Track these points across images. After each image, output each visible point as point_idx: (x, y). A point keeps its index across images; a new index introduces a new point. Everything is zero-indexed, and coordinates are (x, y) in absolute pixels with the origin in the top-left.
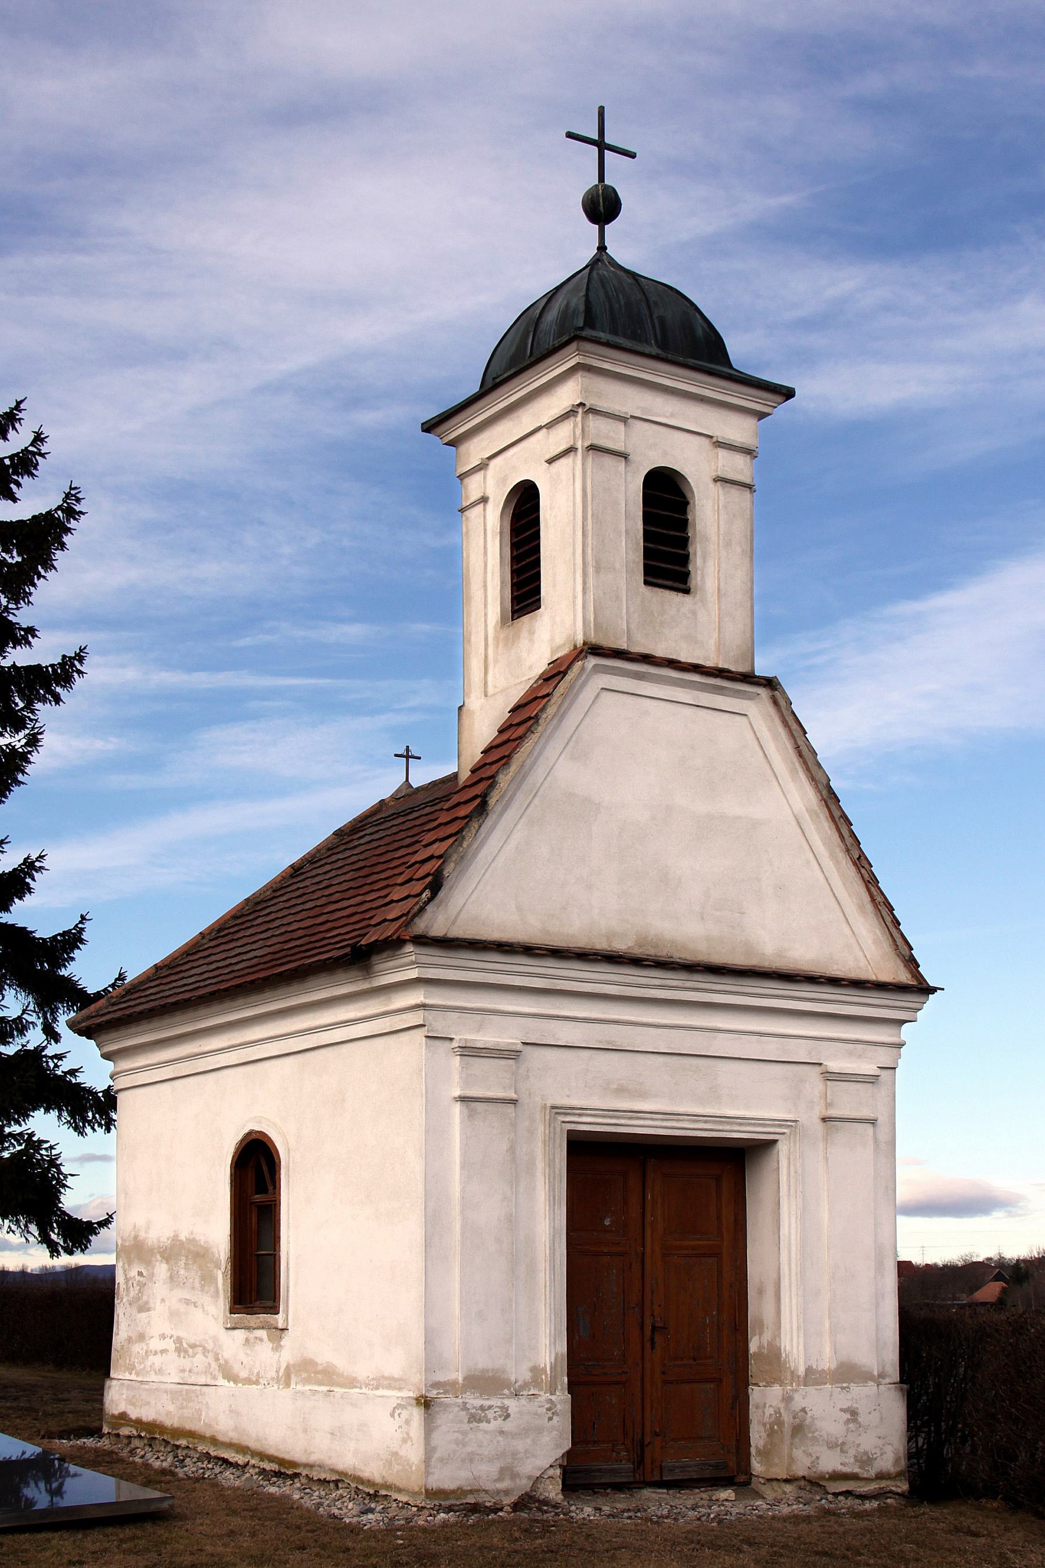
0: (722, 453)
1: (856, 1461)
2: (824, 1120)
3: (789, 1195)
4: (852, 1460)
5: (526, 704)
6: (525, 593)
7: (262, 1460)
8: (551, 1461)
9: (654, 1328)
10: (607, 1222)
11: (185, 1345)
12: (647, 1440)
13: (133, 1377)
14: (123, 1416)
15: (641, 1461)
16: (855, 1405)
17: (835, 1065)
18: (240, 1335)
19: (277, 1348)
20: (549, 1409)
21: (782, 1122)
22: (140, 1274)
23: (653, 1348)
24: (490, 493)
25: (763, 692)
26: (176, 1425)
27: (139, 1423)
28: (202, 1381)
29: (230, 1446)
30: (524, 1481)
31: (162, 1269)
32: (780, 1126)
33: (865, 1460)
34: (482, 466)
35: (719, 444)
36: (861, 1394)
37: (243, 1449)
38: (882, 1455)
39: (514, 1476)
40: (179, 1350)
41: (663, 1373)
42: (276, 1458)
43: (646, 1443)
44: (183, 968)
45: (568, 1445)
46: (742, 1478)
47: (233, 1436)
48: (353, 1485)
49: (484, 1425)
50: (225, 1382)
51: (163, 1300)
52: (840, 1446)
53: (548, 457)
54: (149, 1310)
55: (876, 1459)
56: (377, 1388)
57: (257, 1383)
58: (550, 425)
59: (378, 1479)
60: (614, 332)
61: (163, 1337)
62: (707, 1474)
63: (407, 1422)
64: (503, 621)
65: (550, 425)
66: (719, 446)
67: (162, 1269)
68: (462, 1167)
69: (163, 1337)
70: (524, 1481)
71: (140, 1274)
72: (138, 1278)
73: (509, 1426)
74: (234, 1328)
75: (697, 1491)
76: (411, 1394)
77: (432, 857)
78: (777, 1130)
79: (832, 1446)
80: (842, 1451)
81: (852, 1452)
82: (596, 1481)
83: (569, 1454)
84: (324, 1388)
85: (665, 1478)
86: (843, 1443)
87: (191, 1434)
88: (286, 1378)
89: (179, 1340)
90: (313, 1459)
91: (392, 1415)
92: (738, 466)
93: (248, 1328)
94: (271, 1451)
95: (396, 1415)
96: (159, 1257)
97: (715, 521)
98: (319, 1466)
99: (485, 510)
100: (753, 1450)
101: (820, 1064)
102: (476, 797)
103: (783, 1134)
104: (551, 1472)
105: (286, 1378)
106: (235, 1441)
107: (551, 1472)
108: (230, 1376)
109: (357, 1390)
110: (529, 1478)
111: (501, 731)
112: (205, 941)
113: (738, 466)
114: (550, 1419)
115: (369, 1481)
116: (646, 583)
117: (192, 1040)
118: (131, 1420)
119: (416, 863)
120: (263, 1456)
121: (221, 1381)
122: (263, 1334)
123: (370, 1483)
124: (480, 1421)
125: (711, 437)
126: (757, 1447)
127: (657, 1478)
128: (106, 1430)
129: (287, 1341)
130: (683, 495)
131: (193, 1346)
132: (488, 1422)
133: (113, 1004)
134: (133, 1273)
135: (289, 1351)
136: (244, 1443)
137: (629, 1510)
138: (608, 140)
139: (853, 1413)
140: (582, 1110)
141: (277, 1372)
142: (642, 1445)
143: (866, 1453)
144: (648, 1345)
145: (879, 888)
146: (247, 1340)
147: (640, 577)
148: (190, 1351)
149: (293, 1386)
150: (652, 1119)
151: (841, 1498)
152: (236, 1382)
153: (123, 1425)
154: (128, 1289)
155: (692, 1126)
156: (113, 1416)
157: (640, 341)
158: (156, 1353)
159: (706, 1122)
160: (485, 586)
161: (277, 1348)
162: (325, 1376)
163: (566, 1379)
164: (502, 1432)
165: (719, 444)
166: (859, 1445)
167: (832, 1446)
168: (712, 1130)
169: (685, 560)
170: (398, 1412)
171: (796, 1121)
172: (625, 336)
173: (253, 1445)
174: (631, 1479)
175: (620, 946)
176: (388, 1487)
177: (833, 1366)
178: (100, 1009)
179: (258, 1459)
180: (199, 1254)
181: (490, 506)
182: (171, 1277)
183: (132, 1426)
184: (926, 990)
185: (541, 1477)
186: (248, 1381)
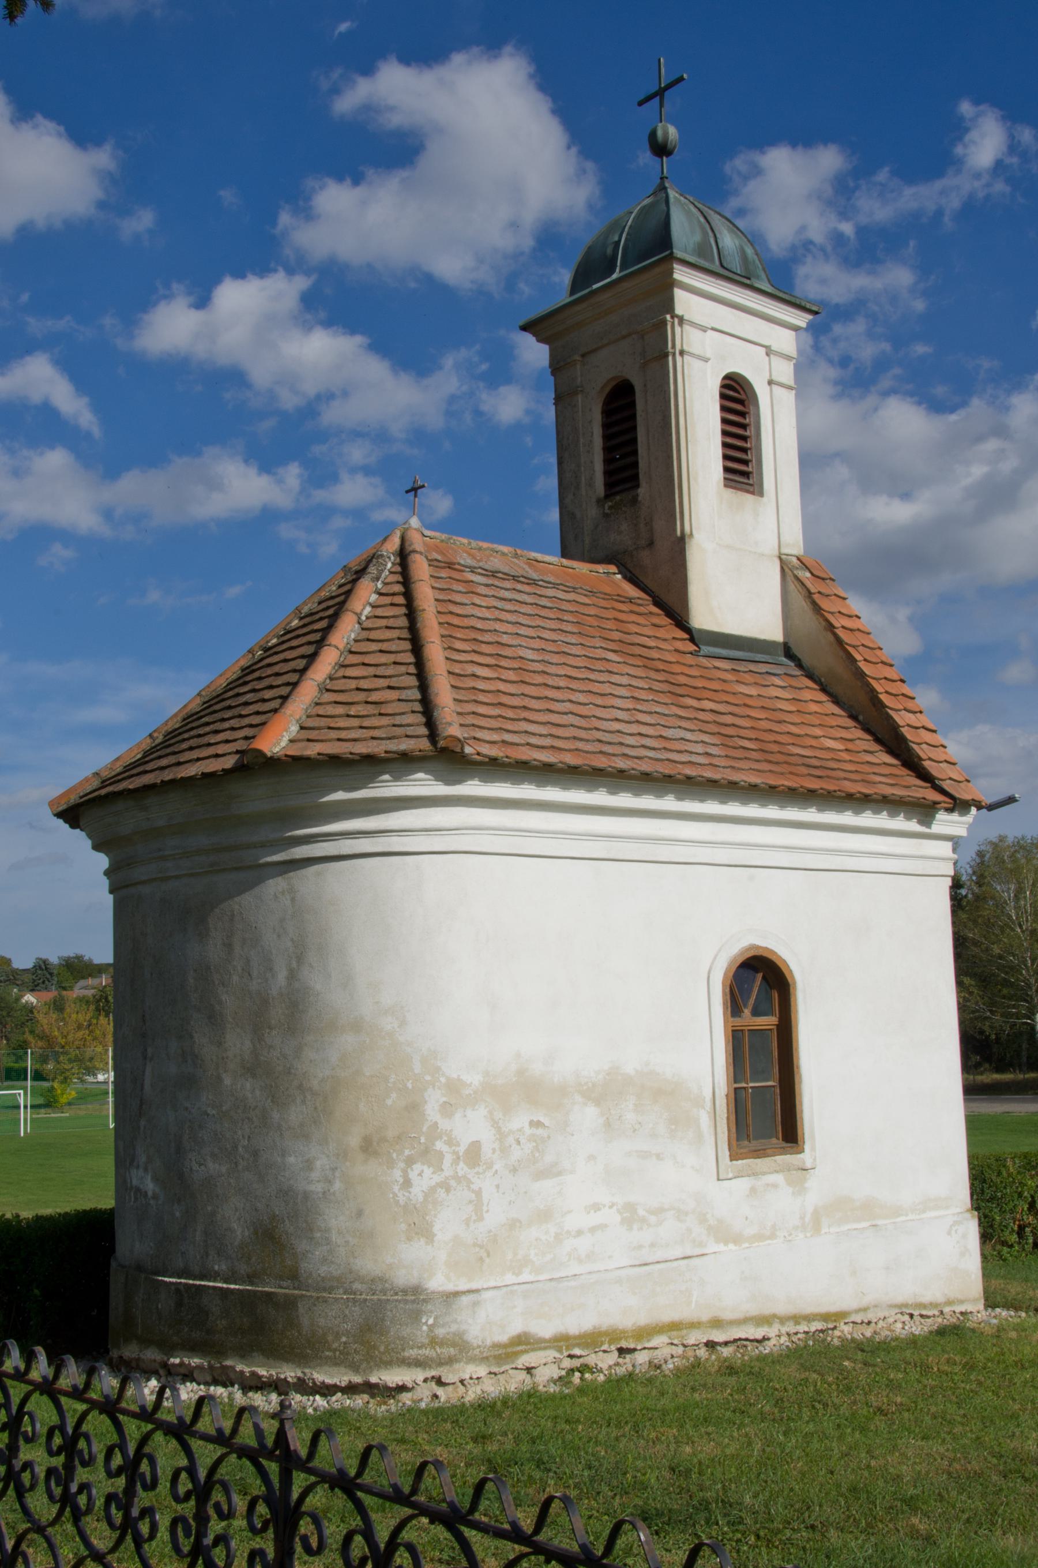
7: (797, 1323)
13: (526, 1277)
18: (742, 1185)
28: (678, 1253)
47: (753, 1309)
48: (916, 1313)
50: (721, 1247)
54: (559, 1174)
56: (924, 1211)
57: (773, 1236)
59: (940, 1298)
63: (964, 1236)
67: (586, 1116)
76: (959, 1210)
88: (815, 1223)
89: (630, 1208)
91: (949, 1233)
94: (809, 1310)
95: (953, 1232)
96: (578, 1098)
98: (876, 1306)
105: (815, 1223)
109: (903, 1218)
115: (931, 1304)
117: (587, 814)
118: (544, 1341)
121: (712, 1247)
123: (933, 1305)
129: (813, 1182)
131: (659, 1211)
135: (818, 1190)
137: (397, 1301)
141: (802, 1218)
146: (753, 1190)
148: (653, 1219)
158: (579, 1233)
162: (867, 1211)
177: (502, 389)
179: (791, 1323)
180: (662, 1092)
182: (608, 1124)
186: (760, 1237)
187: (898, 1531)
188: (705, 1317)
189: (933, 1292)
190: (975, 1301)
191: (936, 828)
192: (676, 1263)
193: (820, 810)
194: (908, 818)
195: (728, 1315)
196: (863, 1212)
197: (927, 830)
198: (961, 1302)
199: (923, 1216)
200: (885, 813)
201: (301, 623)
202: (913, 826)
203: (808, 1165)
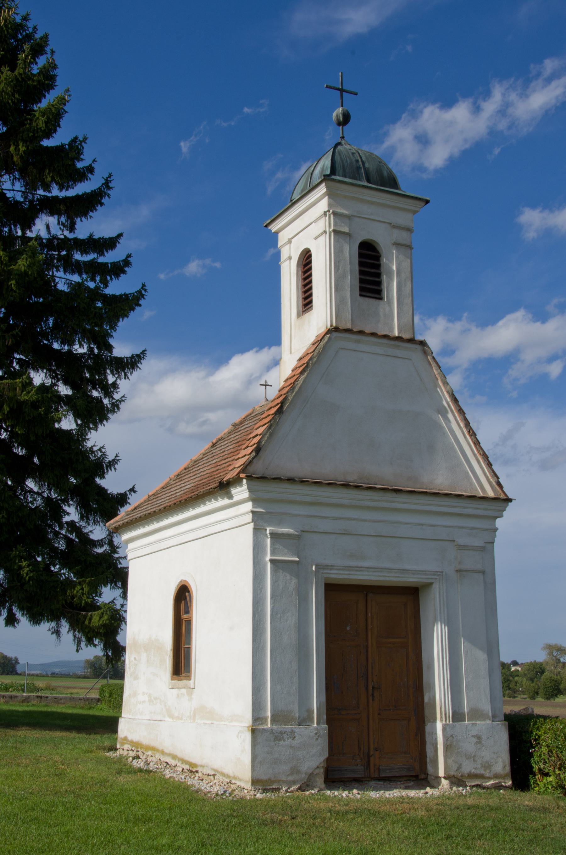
0: (396, 231)
1: (482, 766)
2: (457, 571)
3: (440, 613)
4: (480, 766)
5: (304, 357)
6: (307, 302)
8: (318, 763)
9: (373, 688)
10: (348, 628)
11: (152, 698)
12: (371, 753)
13: (130, 716)
14: (125, 738)
15: (368, 765)
16: (480, 734)
17: (462, 541)
18: (175, 691)
19: (190, 699)
20: (316, 734)
21: (435, 573)
22: (135, 659)
23: (373, 700)
24: (293, 255)
25: (418, 347)
26: (147, 744)
27: (132, 743)
29: (170, 755)
30: (304, 775)
31: (144, 656)
32: (434, 575)
33: (487, 766)
34: (290, 241)
35: (395, 227)
36: (483, 725)
37: (174, 757)
38: (496, 763)
39: (298, 772)
40: (150, 701)
41: (379, 714)
42: (188, 762)
43: (371, 755)
44: (159, 495)
45: (326, 755)
46: (422, 776)
49: (282, 743)
51: (144, 673)
52: (473, 758)
53: (315, 236)
55: (493, 765)
57: (181, 719)
58: (315, 221)
60: (345, 176)
61: (144, 694)
62: (404, 773)
64: (299, 316)
65: (315, 221)
66: (394, 228)
68: (271, 598)
69: (144, 694)
70: (304, 775)
71: (135, 659)
72: (134, 661)
73: (295, 743)
74: (173, 688)
75: (399, 783)
77: (257, 435)
78: (433, 577)
79: (468, 757)
80: (474, 760)
81: (479, 761)
82: (345, 776)
83: (328, 759)
84: (209, 722)
85: (381, 776)
86: (474, 756)
87: (153, 749)
89: (150, 696)
90: (204, 762)
91: (237, 737)
92: (403, 237)
93: (178, 688)
94: (186, 758)
97: (393, 264)
99: (290, 263)
100: (428, 760)
101: (454, 541)
102: (278, 404)
103: (436, 579)
104: (317, 771)
106: (172, 752)
107: (317, 771)
108: (171, 716)
109: (223, 723)
110: (306, 773)
111: (293, 371)
112: (172, 481)
113: (403, 237)
114: (317, 739)
116: (361, 295)
117: (148, 536)
118: (128, 741)
119: (250, 438)
120: (184, 761)
121: (167, 719)
122: (184, 691)
124: (280, 740)
125: (390, 224)
126: (430, 758)
127: (376, 775)
128: (118, 747)
130: (378, 252)
131: (156, 699)
132: (284, 741)
133: (128, 515)
134: (132, 659)
136: (175, 754)
138: (344, 88)
139: (479, 738)
140: (332, 567)
141: (190, 713)
142: (369, 757)
143: (487, 762)
144: (371, 698)
145: (480, 447)
146: (178, 695)
147: (357, 292)
149: (197, 721)
150: (368, 571)
151: (474, 788)
152: (173, 718)
153: (125, 743)
154: (130, 668)
155: (388, 575)
156: (121, 738)
157: (357, 180)
159: (395, 573)
160: (290, 300)
161: (190, 699)
163: (325, 717)
164: (291, 747)
165: (395, 227)
166: (483, 757)
167: (468, 757)
168: (399, 577)
169: (379, 283)
170: (240, 735)
171: (442, 572)
172: (350, 178)
173: (179, 755)
174: (363, 776)
175: (351, 478)
176: (235, 778)
178: (122, 517)
179: (180, 762)
181: (292, 261)
182: (148, 661)
183: (129, 744)
184: (509, 500)
185: (312, 773)
186: (178, 718)
187: (105, 804)
188: (160, 749)
189: (229, 770)
190: (247, 782)
191: (236, 498)
192: (157, 722)
193: (193, 509)
194: (216, 499)
195: (166, 751)
196: (204, 713)
197: (231, 501)
198: (240, 780)
199: (232, 724)
200: (213, 500)
201: (241, 447)
202: (226, 501)
203: (192, 686)
